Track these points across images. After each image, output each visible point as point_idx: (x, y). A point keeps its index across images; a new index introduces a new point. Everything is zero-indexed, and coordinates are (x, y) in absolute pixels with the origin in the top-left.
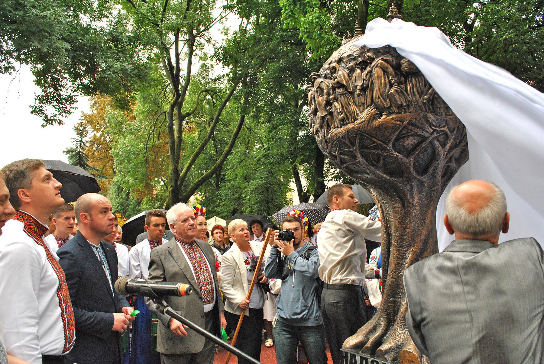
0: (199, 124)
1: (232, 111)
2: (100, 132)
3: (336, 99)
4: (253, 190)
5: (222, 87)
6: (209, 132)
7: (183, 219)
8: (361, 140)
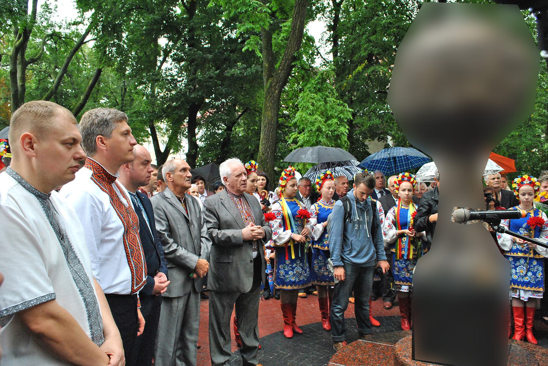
7: (237, 174)
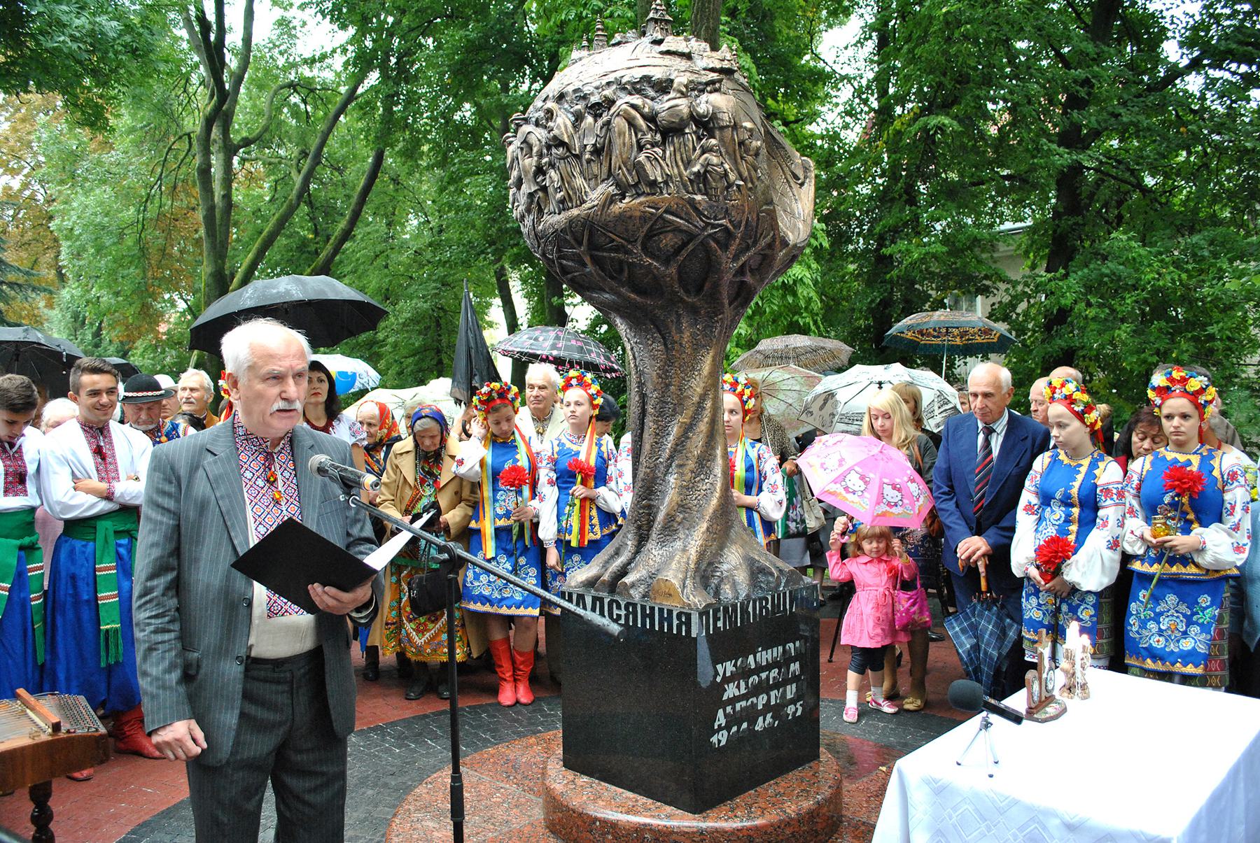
0: (272, 166)
1: (353, 137)
2: (21, 177)
3: (551, 165)
4: (404, 324)
5: (329, 76)
6: (297, 186)
8: (591, 235)
